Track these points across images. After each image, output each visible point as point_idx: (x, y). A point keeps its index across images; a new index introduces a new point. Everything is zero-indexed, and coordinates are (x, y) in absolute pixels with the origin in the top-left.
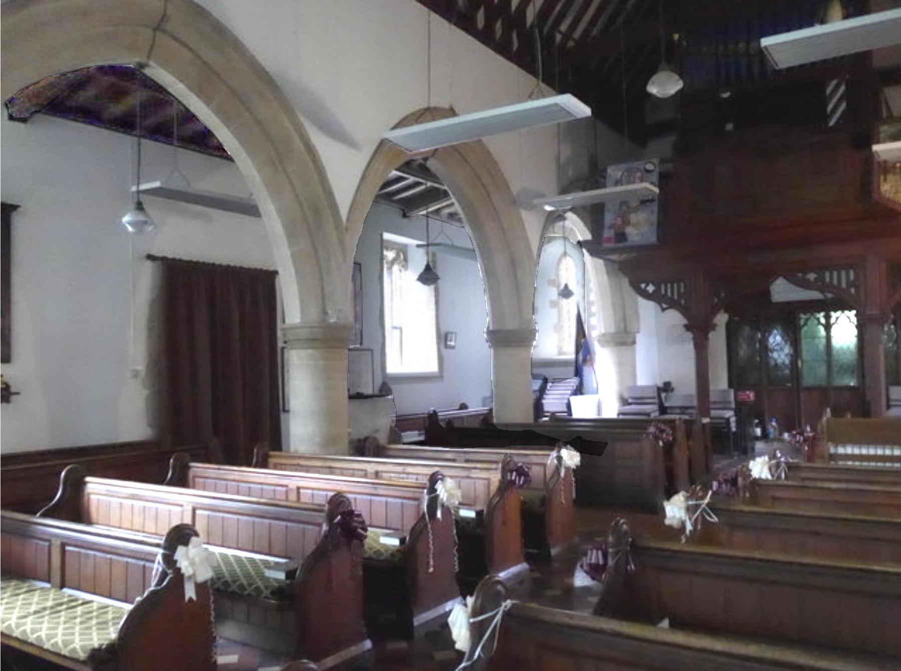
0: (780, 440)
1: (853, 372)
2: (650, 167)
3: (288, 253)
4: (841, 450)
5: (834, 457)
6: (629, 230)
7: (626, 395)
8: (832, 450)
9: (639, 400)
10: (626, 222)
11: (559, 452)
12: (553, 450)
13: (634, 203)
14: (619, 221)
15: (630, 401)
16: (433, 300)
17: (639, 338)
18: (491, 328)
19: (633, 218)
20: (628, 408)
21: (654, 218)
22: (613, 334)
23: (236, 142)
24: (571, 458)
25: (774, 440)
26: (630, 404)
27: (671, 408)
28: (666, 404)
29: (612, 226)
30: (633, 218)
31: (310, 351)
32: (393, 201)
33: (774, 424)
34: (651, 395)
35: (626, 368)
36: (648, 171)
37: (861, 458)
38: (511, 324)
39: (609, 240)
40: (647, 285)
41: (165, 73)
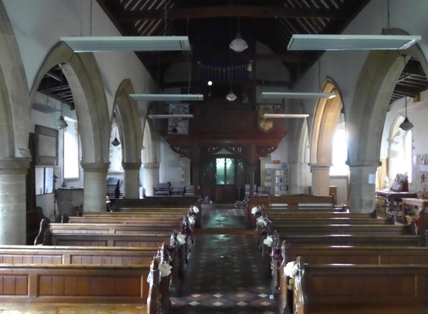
0: (208, 203)
1: (219, 178)
2: (186, 106)
3: (92, 135)
4: (273, 205)
5: (272, 207)
6: (178, 128)
7: (156, 188)
8: (270, 205)
9: (162, 189)
10: (177, 125)
11: (192, 208)
12: (189, 207)
13: (180, 119)
14: (174, 124)
15: (158, 189)
16: (77, 145)
17: (161, 165)
18: (125, 161)
19: (180, 124)
20: (157, 192)
21: (187, 125)
22: (151, 163)
23: (83, 94)
24: (196, 210)
25: (207, 203)
26: (158, 191)
27: (174, 192)
28: (173, 191)
29: (171, 126)
30: (180, 124)
31: (97, 173)
32: (66, 101)
33: (207, 197)
34: (167, 187)
35: (155, 176)
36: (185, 108)
37: (278, 207)
38: (134, 161)
39: (170, 131)
40: (177, 147)
41: (72, 69)
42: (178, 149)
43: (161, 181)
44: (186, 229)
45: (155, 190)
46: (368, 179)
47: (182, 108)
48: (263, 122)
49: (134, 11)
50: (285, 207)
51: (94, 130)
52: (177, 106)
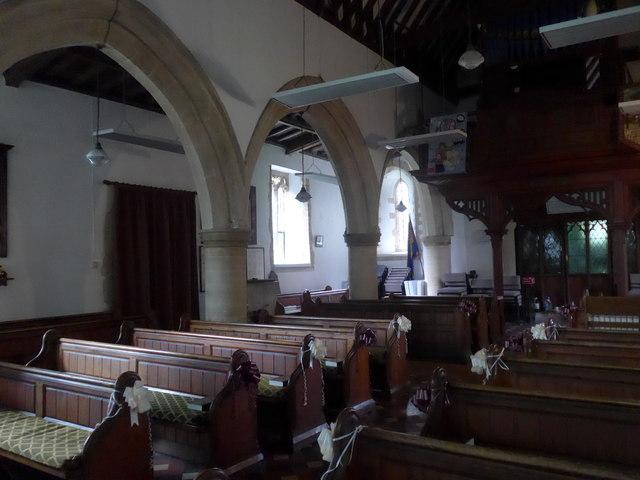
2: (461, 118)
4: (596, 319)
5: (591, 324)
7: (444, 280)
8: (590, 319)
9: (453, 284)
10: (444, 158)
17: (453, 240)
21: (464, 154)
27: (476, 289)
31: (219, 249)
35: (443, 262)
42: (461, 205)
43: (455, 270)
44: (240, 371)
45: (442, 284)
46: (623, 101)
47: (453, 124)
48: (631, 125)
49: (555, 43)
50: (632, 325)
51: (206, 168)
52: (445, 121)
